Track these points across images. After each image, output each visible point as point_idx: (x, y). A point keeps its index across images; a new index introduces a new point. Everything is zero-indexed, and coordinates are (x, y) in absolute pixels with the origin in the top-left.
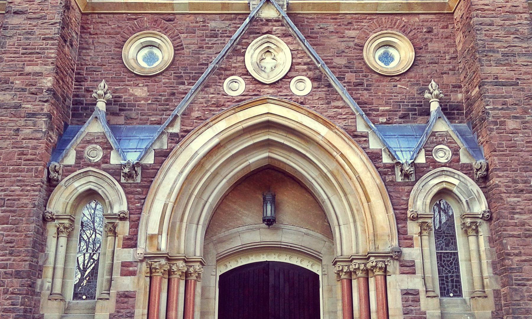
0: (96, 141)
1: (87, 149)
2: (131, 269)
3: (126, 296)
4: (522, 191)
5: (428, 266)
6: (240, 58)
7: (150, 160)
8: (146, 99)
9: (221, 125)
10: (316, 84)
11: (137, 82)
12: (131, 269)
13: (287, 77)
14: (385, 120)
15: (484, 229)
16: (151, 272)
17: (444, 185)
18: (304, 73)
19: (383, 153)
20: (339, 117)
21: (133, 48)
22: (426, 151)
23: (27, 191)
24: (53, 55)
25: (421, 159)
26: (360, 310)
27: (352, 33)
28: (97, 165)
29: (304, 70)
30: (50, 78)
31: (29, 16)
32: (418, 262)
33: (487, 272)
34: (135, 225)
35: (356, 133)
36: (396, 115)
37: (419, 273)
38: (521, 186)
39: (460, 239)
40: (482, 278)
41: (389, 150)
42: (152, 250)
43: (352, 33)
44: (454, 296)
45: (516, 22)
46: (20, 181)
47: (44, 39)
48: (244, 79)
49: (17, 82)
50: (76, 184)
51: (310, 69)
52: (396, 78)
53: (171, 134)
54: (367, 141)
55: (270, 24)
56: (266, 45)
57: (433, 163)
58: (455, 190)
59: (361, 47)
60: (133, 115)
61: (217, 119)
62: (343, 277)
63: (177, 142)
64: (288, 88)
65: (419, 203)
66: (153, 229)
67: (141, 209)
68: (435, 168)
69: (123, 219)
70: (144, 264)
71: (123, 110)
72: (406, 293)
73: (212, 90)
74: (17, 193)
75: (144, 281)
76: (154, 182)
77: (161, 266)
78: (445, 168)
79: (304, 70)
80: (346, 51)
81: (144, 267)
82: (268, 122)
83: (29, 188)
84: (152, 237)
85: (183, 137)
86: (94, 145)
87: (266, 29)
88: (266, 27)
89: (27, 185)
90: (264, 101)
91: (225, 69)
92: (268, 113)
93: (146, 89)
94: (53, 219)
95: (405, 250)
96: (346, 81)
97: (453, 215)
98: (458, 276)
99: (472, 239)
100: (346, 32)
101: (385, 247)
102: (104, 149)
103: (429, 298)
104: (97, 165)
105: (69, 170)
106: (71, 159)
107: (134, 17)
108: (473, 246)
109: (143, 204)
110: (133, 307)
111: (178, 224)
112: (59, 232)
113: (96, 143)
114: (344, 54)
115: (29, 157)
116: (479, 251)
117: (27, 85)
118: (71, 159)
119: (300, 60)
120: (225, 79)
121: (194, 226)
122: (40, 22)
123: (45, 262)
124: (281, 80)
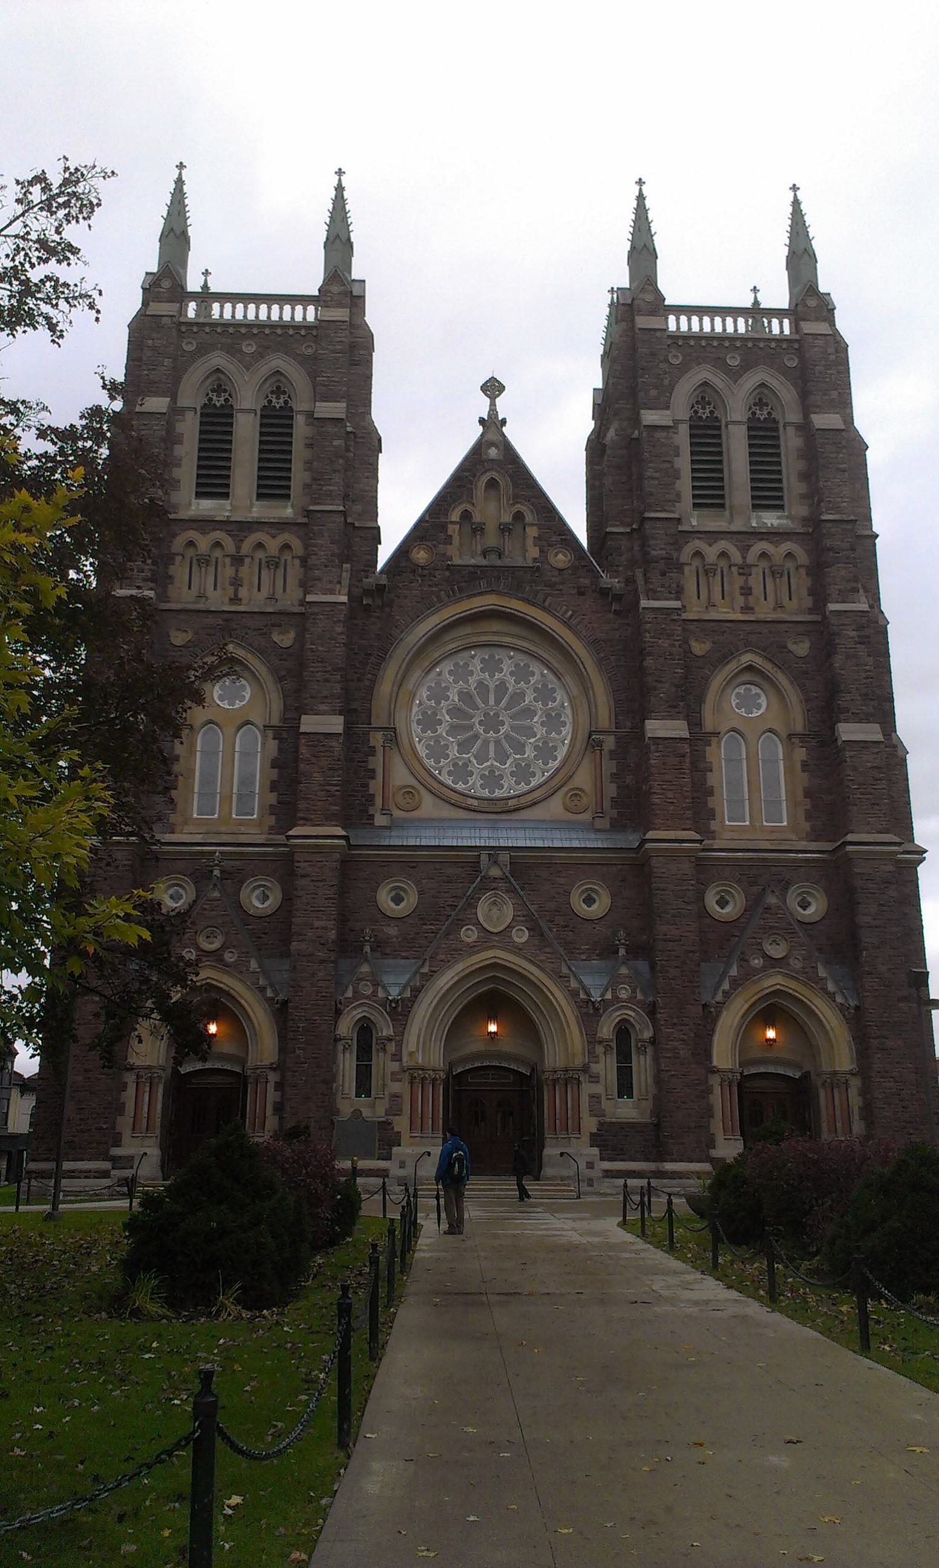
0: (367, 978)
1: (360, 985)
2: (398, 1077)
3: (398, 1097)
4: (675, 1024)
5: (609, 1078)
6: (474, 911)
7: (408, 994)
8: (397, 938)
9: (460, 966)
10: (532, 933)
11: (389, 922)
12: (398, 1077)
13: (510, 927)
14: (585, 958)
15: (650, 1050)
16: (412, 1079)
17: (624, 1016)
18: (523, 924)
19: (581, 991)
20: (549, 960)
21: (385, 892)
22: (612, 989)
23: (325, 1020)
24: (334, 913)
25: (609, 996)
26: (561, 1108)
27: (562, 881)
28: (368, 997)
29: (523, 922)
30: (333, 932)
31: (314, 878)
32: (602, 1074)
33: (650, 1081)
34: (400, 1045)
35: (561, 974)
36: (593, 953)
37: (602, 1081)
38: (675, 1020)
39: (634, 1057)
40: (647, 1086)
41: (584, 988)
42: (412, 1064)
43: (562, 881)
44: (627, 1098)
45: (684, 888)
46: (319, 1013)
47: (326, 899)
48: (476, 928)
49: (310, 934)
50: (355, 1013)
51: (526, 921)
52: (595, 921)
53: (422, 973)
54: (569, 981)
55: (497, 881)
56: (493, 899)
57: (616, 998)
58: (632, 1020)
59: (568, 893)
60: (388, 950)
61: (457, 962)
62: (549, 1083)
63: (427, 981)
64: (510, 937)
65: (605, 1030)
66: (412, 1047)
67: (403, 1033)
68: (619, 1002)
69: (390, 1040)
70: (407, 1074)
71: (379, 947)
72: (592, 1096)
73: (452, 938)
74: (318, 1021)
75: (407, 1086)
76: (412, 1012)
77: (419, 1075)
78: (625, 1004)
79: (523, 922)
80: (557, 896)
81: (407, 1075)
82: (495, 963)
83: (327, 1018)
84: (411, 1054)
85: (432, 976)
86: (366, 982)
87: (494, 885)
88: (493, 884)
89: (324, 1016)
90: (493, 947)
91: (462, 921)
92: (495, 957)
93: (396, 928)
94: (340, 1040)
95: (593, 1066)
96: (556, 923)
97: (710, 962)
98: (632, 1084)
99: (642, 1057)
100: (558, 879)
101: (578, 1062)
102: (373, 985)
103: (608, 1101)
104: (368, 997)
105: (349, 1001)
106: (349, 993)
107: (384, 864)
108: (642, 1062)
109: (405, 1028)
110: (402, 1104)
111: (428, 1042)
112: (345, 1049)
113: (367, 980)
114: (555, 899)
115: (324, 994)
116: (646, 1066)
117: (318, 937)
118: (349, 993)
119: (519, 913)
120: (462, 928)
121: (439, 1042)
122: (323, 883)
123: (337, 1071)
124: (505, 929)
